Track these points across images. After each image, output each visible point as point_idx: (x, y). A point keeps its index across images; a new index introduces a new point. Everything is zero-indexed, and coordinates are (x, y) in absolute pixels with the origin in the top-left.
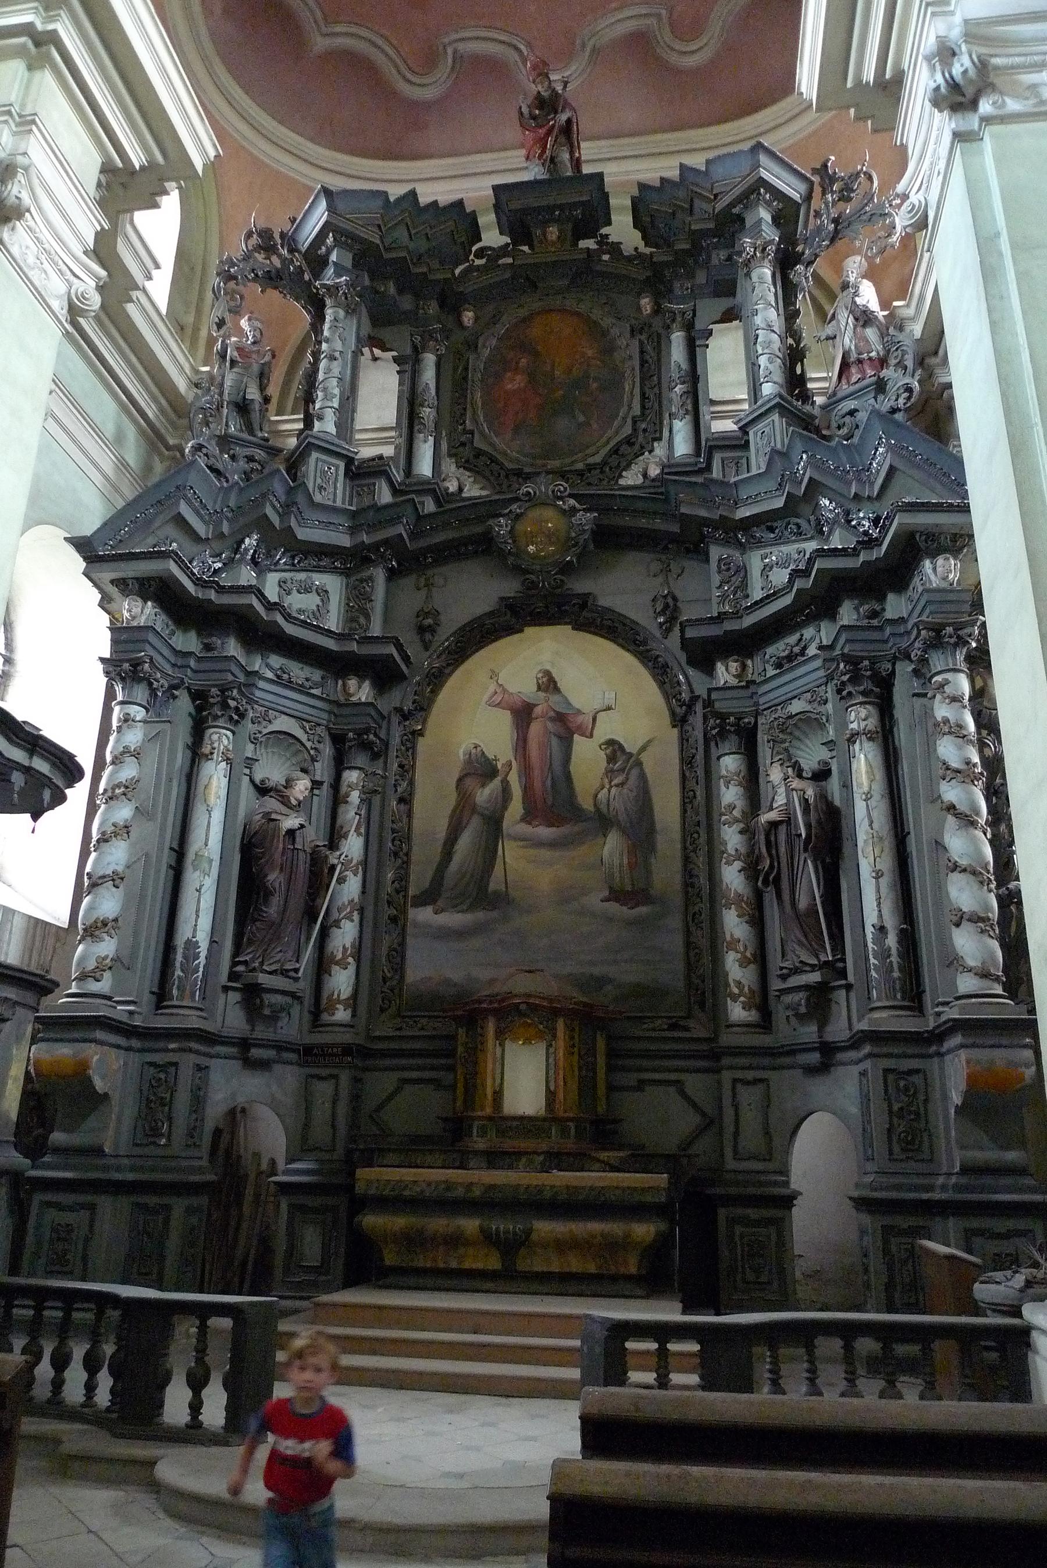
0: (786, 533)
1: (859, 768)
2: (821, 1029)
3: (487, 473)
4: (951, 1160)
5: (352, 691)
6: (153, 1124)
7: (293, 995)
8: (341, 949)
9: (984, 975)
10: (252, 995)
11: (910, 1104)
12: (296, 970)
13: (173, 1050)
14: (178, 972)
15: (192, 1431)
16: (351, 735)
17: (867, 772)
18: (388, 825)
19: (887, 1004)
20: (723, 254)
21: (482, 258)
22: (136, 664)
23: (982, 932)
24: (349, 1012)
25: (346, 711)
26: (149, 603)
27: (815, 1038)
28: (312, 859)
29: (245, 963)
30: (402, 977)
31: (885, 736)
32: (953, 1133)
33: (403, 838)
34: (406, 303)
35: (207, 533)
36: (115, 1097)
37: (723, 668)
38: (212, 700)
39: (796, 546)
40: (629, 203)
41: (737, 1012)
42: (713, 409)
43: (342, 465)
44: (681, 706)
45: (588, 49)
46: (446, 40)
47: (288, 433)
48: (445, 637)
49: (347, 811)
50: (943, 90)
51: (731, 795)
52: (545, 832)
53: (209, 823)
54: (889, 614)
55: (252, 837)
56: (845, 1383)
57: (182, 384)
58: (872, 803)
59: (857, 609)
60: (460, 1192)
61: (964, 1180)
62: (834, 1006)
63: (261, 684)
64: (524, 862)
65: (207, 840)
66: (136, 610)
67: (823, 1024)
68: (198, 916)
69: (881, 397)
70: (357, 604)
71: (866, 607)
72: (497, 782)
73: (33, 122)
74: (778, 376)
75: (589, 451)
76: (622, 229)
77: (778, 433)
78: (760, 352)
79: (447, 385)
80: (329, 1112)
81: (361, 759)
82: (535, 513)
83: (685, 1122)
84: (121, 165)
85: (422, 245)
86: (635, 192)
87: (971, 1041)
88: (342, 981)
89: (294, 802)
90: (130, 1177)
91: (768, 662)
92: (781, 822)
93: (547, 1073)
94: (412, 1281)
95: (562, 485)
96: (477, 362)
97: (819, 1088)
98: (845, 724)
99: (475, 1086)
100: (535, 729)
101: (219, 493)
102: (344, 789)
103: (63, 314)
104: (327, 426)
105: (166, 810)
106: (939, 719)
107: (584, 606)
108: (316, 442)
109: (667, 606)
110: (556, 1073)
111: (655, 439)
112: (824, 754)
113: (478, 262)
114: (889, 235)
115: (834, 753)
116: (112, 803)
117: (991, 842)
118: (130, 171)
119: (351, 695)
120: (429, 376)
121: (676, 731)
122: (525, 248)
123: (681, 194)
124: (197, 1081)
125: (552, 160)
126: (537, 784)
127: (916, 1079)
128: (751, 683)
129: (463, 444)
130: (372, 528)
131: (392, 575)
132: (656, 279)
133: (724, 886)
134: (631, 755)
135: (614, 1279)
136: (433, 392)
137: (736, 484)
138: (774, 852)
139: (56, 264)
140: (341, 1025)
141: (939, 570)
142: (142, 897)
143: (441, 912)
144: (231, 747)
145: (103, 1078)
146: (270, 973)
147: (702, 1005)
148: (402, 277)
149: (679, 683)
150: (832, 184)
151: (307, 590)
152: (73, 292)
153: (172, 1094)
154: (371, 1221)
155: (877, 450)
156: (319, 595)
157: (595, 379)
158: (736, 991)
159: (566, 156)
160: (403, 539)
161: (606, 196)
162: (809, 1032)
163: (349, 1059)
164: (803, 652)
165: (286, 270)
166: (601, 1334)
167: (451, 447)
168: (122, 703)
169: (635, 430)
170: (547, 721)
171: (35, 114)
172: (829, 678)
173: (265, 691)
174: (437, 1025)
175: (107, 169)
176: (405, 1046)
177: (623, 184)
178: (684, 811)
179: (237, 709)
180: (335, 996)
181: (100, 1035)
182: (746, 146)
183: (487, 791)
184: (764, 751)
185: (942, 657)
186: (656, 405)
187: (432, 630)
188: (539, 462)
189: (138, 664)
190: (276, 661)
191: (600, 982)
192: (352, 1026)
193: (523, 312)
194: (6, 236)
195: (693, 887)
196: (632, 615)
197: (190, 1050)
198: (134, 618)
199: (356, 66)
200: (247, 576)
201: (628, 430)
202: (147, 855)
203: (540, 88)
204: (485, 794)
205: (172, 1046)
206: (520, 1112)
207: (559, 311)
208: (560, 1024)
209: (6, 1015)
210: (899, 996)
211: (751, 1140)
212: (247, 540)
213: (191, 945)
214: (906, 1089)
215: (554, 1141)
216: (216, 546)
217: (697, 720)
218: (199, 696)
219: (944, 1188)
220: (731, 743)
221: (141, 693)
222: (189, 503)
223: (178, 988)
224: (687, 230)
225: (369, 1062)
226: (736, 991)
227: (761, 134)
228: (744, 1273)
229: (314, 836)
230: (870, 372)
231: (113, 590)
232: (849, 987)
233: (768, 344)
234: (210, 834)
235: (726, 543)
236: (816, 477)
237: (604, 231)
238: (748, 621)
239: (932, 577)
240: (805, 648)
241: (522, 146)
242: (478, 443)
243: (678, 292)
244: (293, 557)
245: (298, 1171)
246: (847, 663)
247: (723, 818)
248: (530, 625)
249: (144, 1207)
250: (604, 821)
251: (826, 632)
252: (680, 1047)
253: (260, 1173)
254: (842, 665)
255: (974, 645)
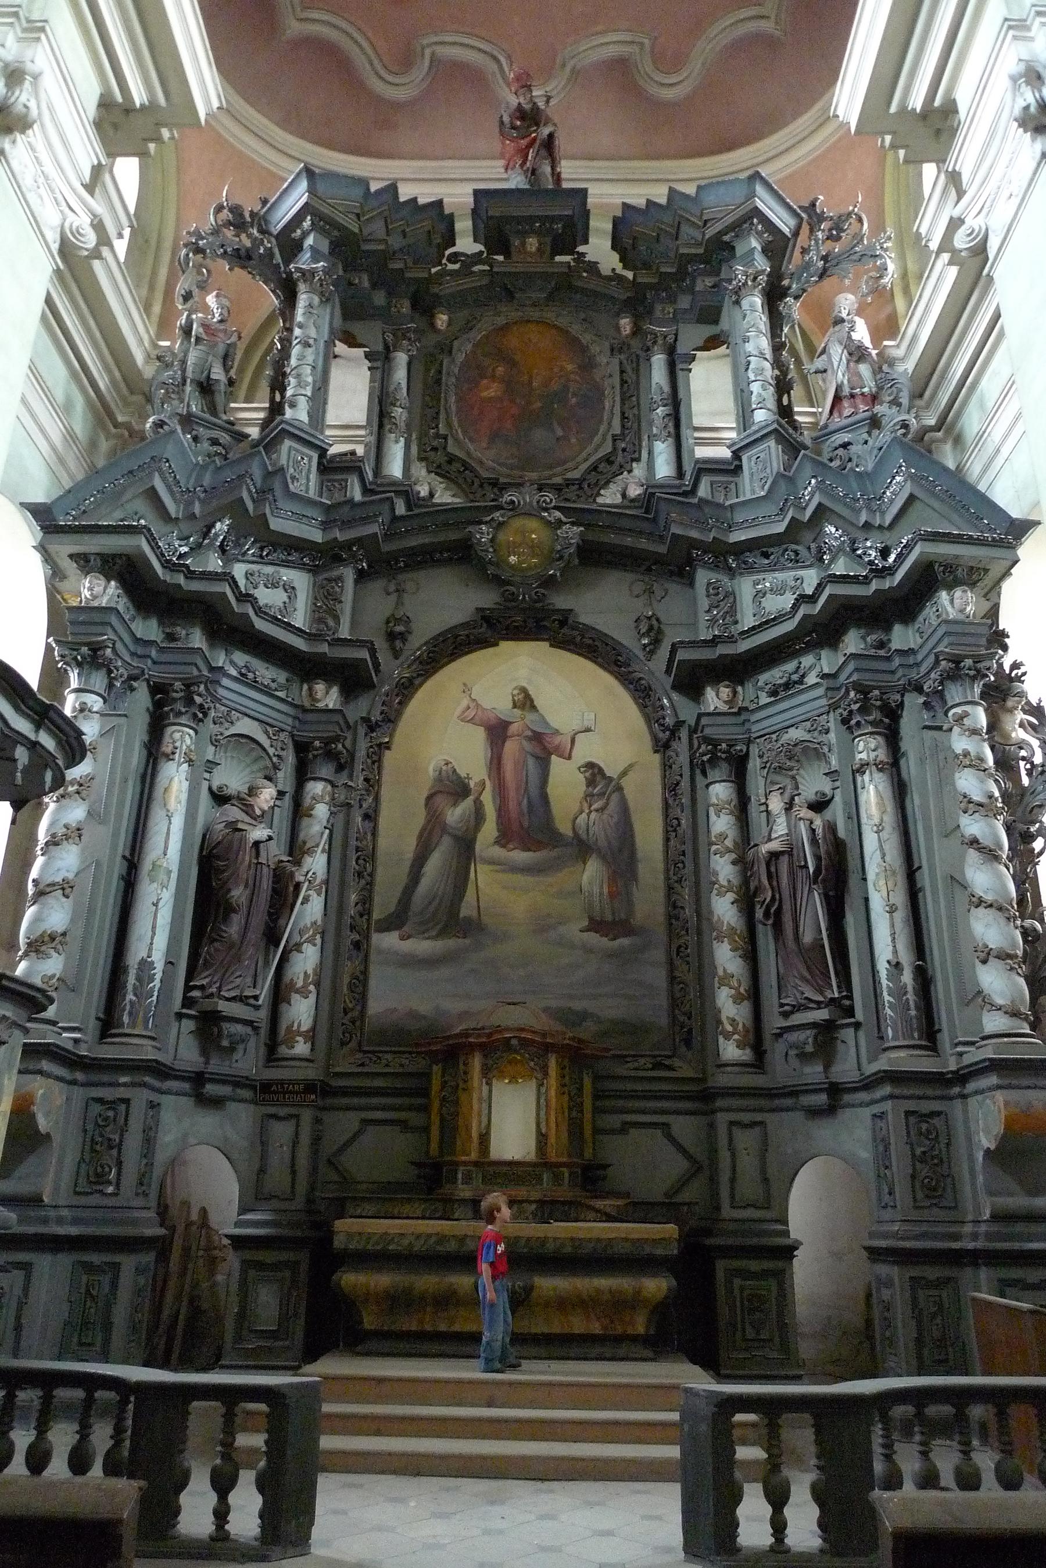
0: (782, 560)
1: (868, 798)
2: (827, 1067)
3: (461, 481)
4: (977, 1208)
5: (319, 695)
6: (99, 1170)
7: (249, 1023)
8: (302, 976)
9: (1015, 1014)
10: (209, 1025)
11: (932, 1148)
12: (256, 998)
13: (125, 1085)
14: (130, 996)
15: (219, 1544)
16: (317, 743)
17: (878, 803)
18: (353, 843)
19: (906, 1043)
20: (709, 281)
21: (455, 263)
22: (96, 649)
23: (1012, 969)
24: (309, 1045)
25: (310, 717)
26: (113, 583)
27: (820, 1078)
28: (275, 875)
29: (202, 988)
30: (364, 1007)
31: (893, 765)
32: (980, 1179)
33: (368, 856)
34: (379, 298)
35: (177, 512)
36: (57, 1139)
37: (713, 694)
38: (175, 695)
39: (792, 573)
40: (609, 226)
41: (731, 1051)
42: (697, 435)
43: (315, 456)
44: (664, 731)
45: (568, 69)
46: (425, 42)
47: (249, 422)
48: (417, 645)
49: (310, 826)
50: (1032, 109)
51: (722, 824)
52: (520, 856)
53: (169, 829)
54: (896, 644)
55: (214, 848)
56: (961, 1455)
57: (139, 358)
58: (884, 835)
59: (863, 638)
60: (452, 1246)
61: (995, 1228)
62: (840, 1047)
63: (225, 682)
64: (497, 886)
65: (166, 848)
66: (98, 589)
67: (827, 1067)
68: (154, 933)
69: (875, 432)
70: (325, 603)
71: (874, 637)
72: (469, 801)
73: (42, 30)
74: (771, 403)
75: (570, 465)
76: (599, 249)
77: (774, 458)
78: (752, 378)
79: (418, 387)
80: (287, 1157)
81: (326, 770)
82: (518, 523)
83: (674, 1166)
84: (120, 99)
85: (396, 242)
86: (619, 214)
87: (1006, 1082)
88: (301, 1011)
89: (258, 812)
90: (74, 1231)
91: (762, 689)
92: (782, 853)
93: (538, 1115)
94: (435, 1348)
95: (549, 496)
96: (453, 366)
97: (824, 1131)
98: (852, 752)
99: (456, 1129)
100: (511, 748)
101: (193, 470)
102: (307, 801)
103: (55, 247)
104: (298, 414)
105: (119, 816)
106: (959, 751)
107: (563, 623)
108: (292, 430)
109: (651, 628)
110: (547, 1113)
111: (633, 460)
112: (825, 786)
113: (451, 267)
114: (881, 277)
115: (838, 784)
116: (64, 802)
117: (1014, 877)
118: (128, 109)
119: (318, 701)
120: (400, 375)
121: (657, 756)
122: (501, 258)
123: (668, 218)
124: (149, 1120)
125: (534, 172)
126: (512, 805)
127: (935, 1121)
128: (743, 710)
129: (435, 449)
130: (346, 524)
131: (361, 576)
132: (638, 302)
133: (716, 918)
134: (610, 779)
135: (619, 1340)
136: (405, 391)
137: (731, 506)
138: (775, 883)
139: (53, 192)
140: (301, 1059)
141: (957, 602)
142: (91, 910)
143: (409, 937)
144: (193, 747)
145: (47, 1115)
146: (228, 999)
147: (688, 1042)
148: (378, 272)
149: (662, 707)
150: (820, 222)
151: (275, 586)
152: (67, 225)
153: (122, 1135)
154: (350, 1279)
155: (894, 478)
156: (286, 590)
157: (574, 395)
158: (730, 1028)
159: (548, 169)
160: (376, 541)
161: (586, 214)
162: (813, 1072)
163: (313, 1097)
164: (801, 681)
165: (258, 249)
166: (707, 1410)
167: (421, 450)
168: (77, 691)
169: (615, 449)
170: (522, 740)
171: (45, 21)
172: (834, 707)
173: (229, 689)
174: (404, 1061)
175: (105, 104)
176: (367, 1083)
177: (602, 206)
178: (667, 840)
179: (201, 706)
180: (295, 1028)
181: (46, 1065)
182: (743, 176)
183: (459, 811)
184: (756, 784)
185: (960, 689)
186: (635, 425)
187: (403, 637)
188: (516, 472)
189: (99, 649)
190: (241, 658)
191: (583, 1016)
192: (311, 1061)
193: (501, 321)
194: (7, 146)
195: (677, 919)
196: (615, 635)
197: (144, 1085)
198: (95, 597)
199: (329, 57)
200: (214, 563)
201: (608, 448)
202: (98, 864)
203: (522, 100)
204: (455, 814)
205: (123, 1079)
206: (508, 1156)
207: (538, 322)
208: (553, 1062)
209: (5, 1037)
210: (916, 1035)
211: (749, 1188)
212: (218, 525)
213: (146, 965)
214: (928, 1131)
215: (546, 1188)
216: (185, 527)
217: (681, 748)
218: (159, 691)
219: (975, 1236)
220: (722, 770)
221: (99, 681)
222: (164, 479)
223: (130, 1014)
224: (672, 255)
225: (329, 1101)
226: (730, 1028)
227: (758, 165)
228: (744, 1329)
229: (276, 852)
230: (862, 407)
231: (70, 567)
232: (857, 1025)
233: (760, 371)
234: (169, 843)
235: (715, 567)
236: (827, 503)
237: (581, 249)
238: (744, 646)
239: (949, 609)
240: (803, 676)
241: (502, 156)
242: (452, 448)
243: (658, 313)
244: (262, 549)
245: (259, 1223)
246: (858, 692)
247: (714, 848)
248: (504, 639)
249: (89, 1268)
250: (582, 848)
251: (827, 661)
252: (686, 1088)
253: (189, 1225)
254: (852, 694)
255: (992, 678)
